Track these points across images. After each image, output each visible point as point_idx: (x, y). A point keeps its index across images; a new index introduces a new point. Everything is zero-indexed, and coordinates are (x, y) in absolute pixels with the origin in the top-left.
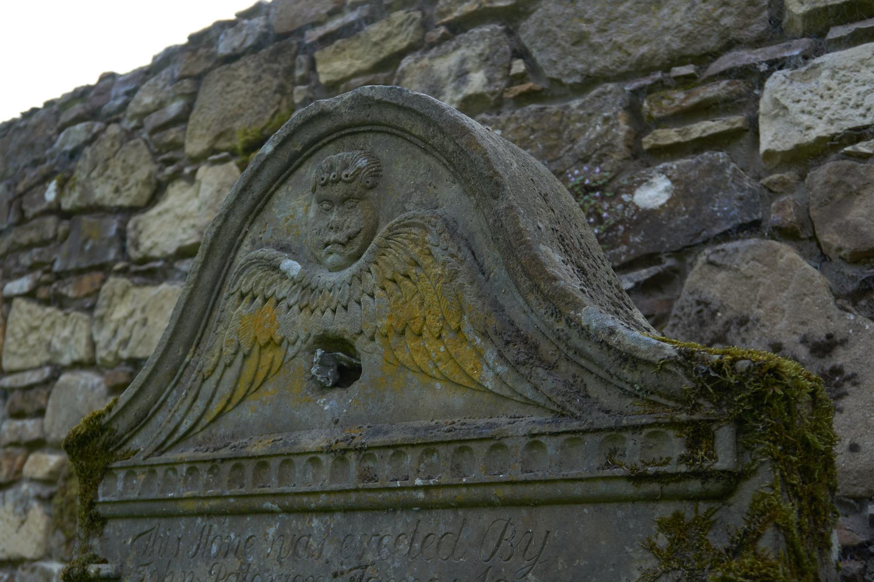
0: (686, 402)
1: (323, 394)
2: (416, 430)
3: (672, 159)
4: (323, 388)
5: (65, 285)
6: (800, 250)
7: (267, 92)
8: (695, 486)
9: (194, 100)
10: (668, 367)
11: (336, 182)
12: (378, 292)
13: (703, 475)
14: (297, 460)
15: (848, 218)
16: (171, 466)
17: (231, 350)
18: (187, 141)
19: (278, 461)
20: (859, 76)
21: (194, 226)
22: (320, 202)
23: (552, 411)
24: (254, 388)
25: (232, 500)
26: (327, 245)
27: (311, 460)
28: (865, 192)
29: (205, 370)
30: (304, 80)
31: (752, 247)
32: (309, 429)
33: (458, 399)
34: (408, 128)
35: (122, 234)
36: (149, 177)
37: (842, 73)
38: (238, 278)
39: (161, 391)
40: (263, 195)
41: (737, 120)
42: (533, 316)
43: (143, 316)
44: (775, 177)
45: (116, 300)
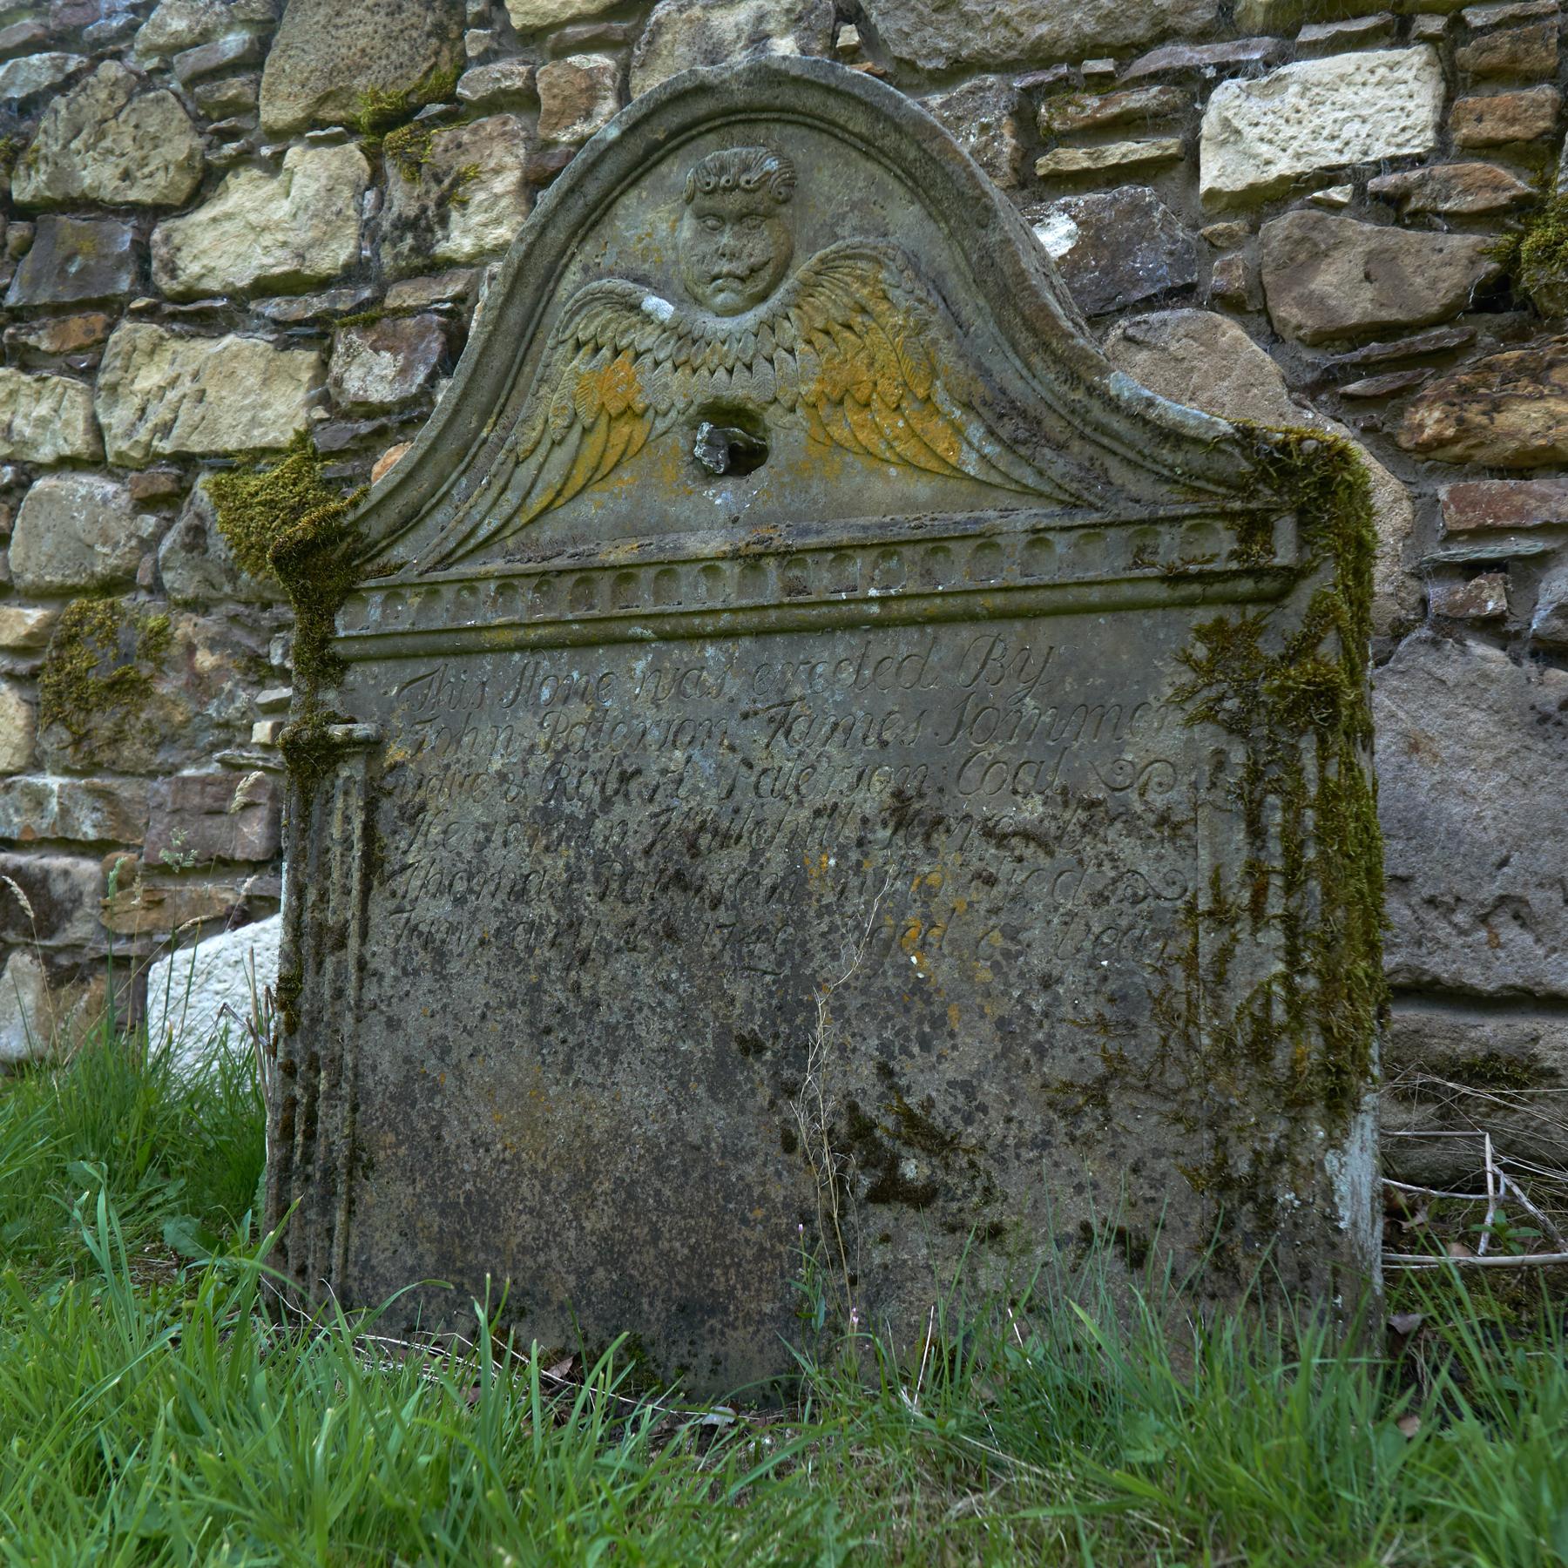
0: (1243, 488)
1: (709, 484)
2: (865, 528)
3: (1076, 193)
4: (709, 476)
5: (32, 330)
6: (1245, 327)
7: (415, 34)
8: (1246, 586)
9: (273, 33)
10: (1223, 446)
11: (729, 190)
12: (800, 346)
13: (1256, 573)
14: (682, 569)
15: (1313, 286)
16: (469, 583)
17: (562, 422)
18: (262, 102)
19: (652, 572)
20: (1336, 97)
21: (284, 244)
22: (701, 216)
23: (1061, 502)
24: (598, 475)
25: (576, 627)
26: (715, 278)
27: (704, 569)
28: (1336, 254)
29: (520, 449)
30: (482, 21)
31: (1185, 319)
32: (693, 530)
33: (922, 489)
34: (841, 121)
35: (142, 251)
36: (190, 157)
37: (1315, 90)
38: (571, 319)
39: (443, 478)
40: (601, 200)
41: (1171, 144)
42: (1035, 383)
43: (197, 386)
44: (1221, 226)
45: (138, 358)
